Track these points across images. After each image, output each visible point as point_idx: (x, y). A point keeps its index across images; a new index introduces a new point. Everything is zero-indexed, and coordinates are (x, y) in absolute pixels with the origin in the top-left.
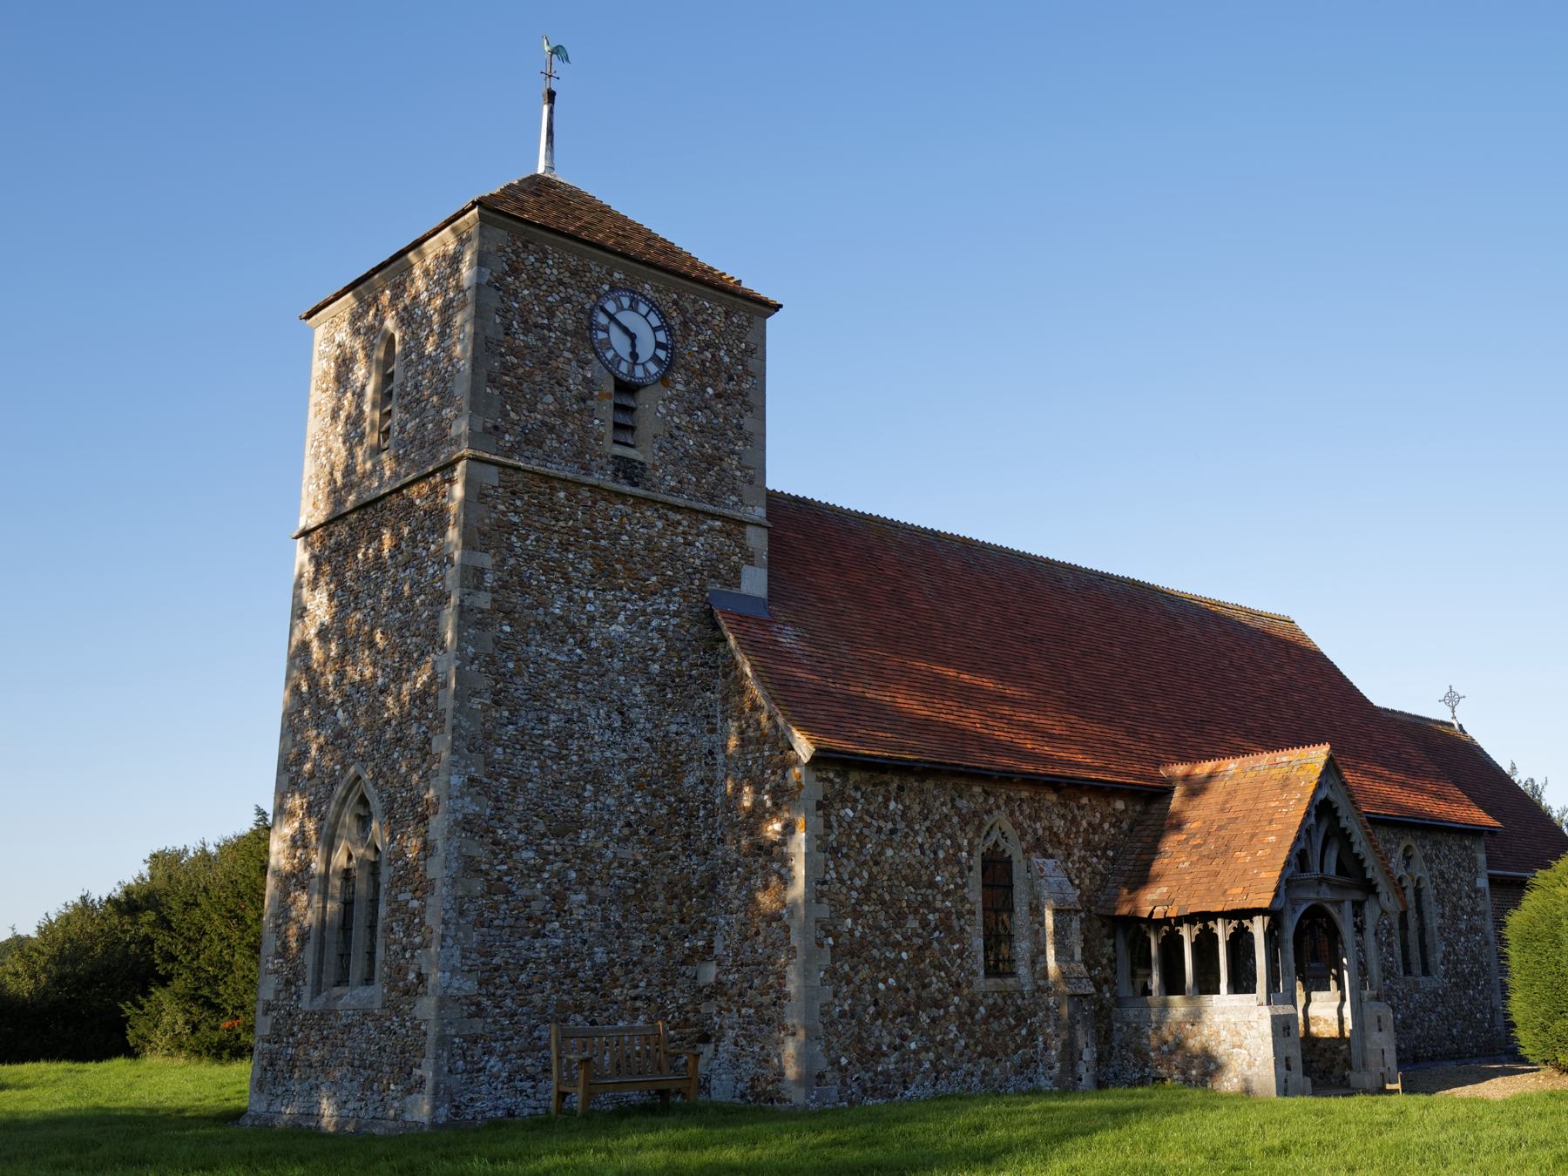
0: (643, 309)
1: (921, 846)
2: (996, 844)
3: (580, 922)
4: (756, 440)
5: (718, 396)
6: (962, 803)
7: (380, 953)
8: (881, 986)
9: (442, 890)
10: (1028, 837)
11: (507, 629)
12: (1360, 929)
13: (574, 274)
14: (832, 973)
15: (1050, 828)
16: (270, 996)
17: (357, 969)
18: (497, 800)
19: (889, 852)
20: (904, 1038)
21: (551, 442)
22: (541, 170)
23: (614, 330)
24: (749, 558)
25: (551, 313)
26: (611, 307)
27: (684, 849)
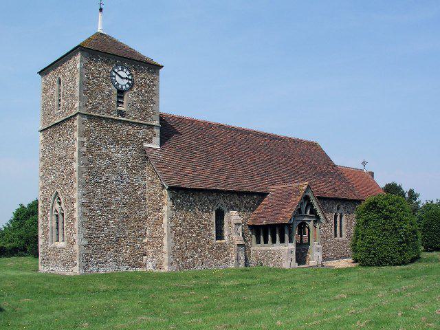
0: (125, 70)
2: (220, 208)
7: (65, 234)
14: (175, 239)
17: (61, 239)
22: (99, 31)
23: (117, 76)
24: (154, 135)
25: (100, 73)
26: (116, 70)
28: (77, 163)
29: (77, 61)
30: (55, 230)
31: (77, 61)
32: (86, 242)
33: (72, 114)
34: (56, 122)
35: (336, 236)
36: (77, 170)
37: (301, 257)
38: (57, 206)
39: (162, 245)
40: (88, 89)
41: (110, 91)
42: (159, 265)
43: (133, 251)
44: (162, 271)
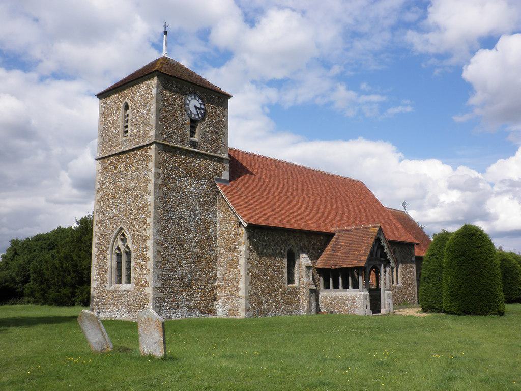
1: (272, 249)
3: (185, 268)
4: (225, 134)
5: (216, 122)
6: (283, 237)
7: (132, 275)
8: (263, 286)
9: (151, 259)
10: (299, 247)
11: (166, 189)
12: (385, 272)
13: (180, 89)
15: (304, 244)
16: (95, 286)
17: (124, 278)
18: (165, 236)
19: (265, 251)
20: (268, 300)
21: (175, 137)
24: (224, 169)
25: (174, 100)
27: (209, 249)
28: (152, 196)
29: (153, 84)
30: (115, 271)
31: (153, 84)
32: (159, 285)
33: (145, 143)
34: (121, 150)
35: (393, 283)
36: (153, 204)
37: (375, 303)
38: (120, 244)
39: (238, 289)
40: (163, 118)
41: (184, 120)
42: (234, 311)
43: (203, 295)
44: (238, 317)
